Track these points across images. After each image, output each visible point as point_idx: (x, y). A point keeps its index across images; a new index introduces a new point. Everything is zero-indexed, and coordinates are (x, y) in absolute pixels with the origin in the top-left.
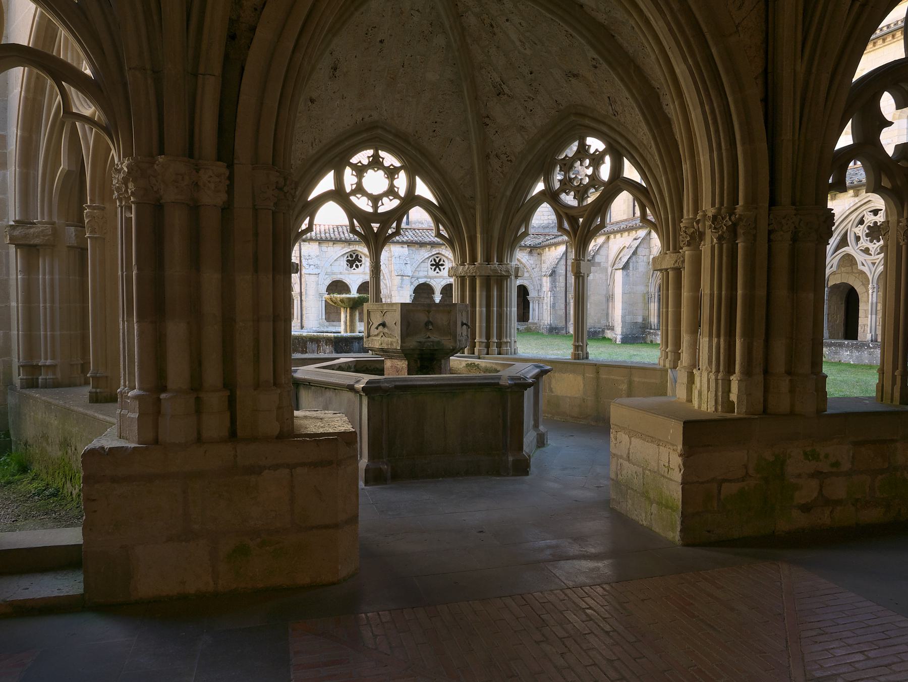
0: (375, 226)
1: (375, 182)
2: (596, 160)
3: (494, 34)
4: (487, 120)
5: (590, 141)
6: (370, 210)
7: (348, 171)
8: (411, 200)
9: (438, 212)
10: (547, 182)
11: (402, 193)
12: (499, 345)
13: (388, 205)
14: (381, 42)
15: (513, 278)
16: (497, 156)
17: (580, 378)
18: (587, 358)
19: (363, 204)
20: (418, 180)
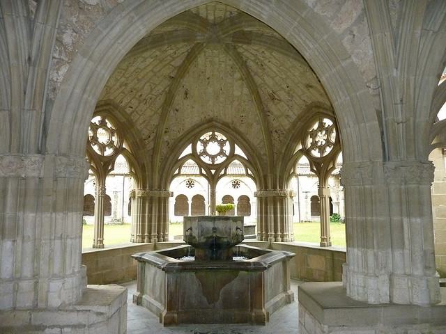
0: (213, 171)
1: (213, 148)
3: (264, 69)
4: (269, 114)
6: (211, 163)
7: (199, 143)
8: (232, 156)
9: (248, 163)
10: (303, 144)
11: (228, 154)
12: (282, 236)
13: (220, 160)
14: (208, 78)
15: (289, 197)
16: (276, 131)
17: (323, 259)
18: (330, 246)
19: (206, 160)
20: (236, 146)
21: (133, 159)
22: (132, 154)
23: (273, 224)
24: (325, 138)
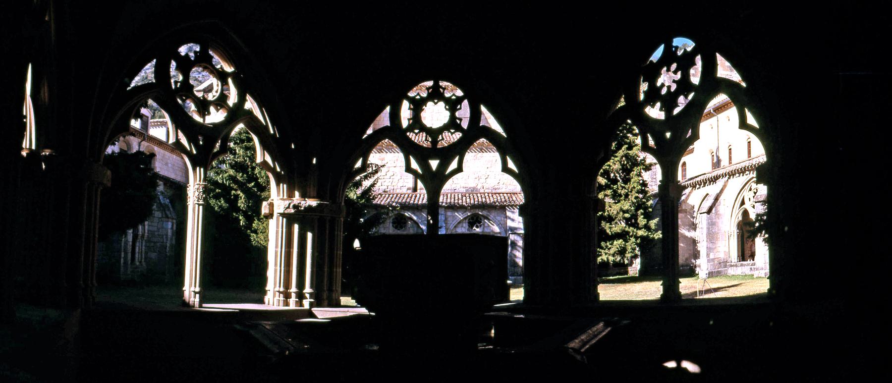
0: (434, 164)
1: (435, 115)
2: (686, 63)
5: (678, 42)
11: (465, 125)
19: (420, 139)
24: (679, 76)
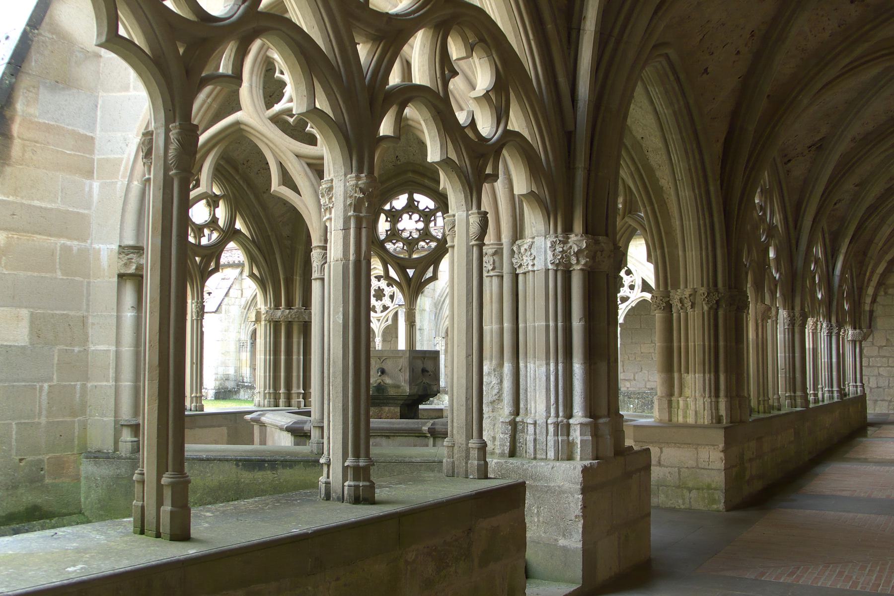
0: (411, 272)
21: (255, 252)
22: (253, 241)
23: (295, 374)
